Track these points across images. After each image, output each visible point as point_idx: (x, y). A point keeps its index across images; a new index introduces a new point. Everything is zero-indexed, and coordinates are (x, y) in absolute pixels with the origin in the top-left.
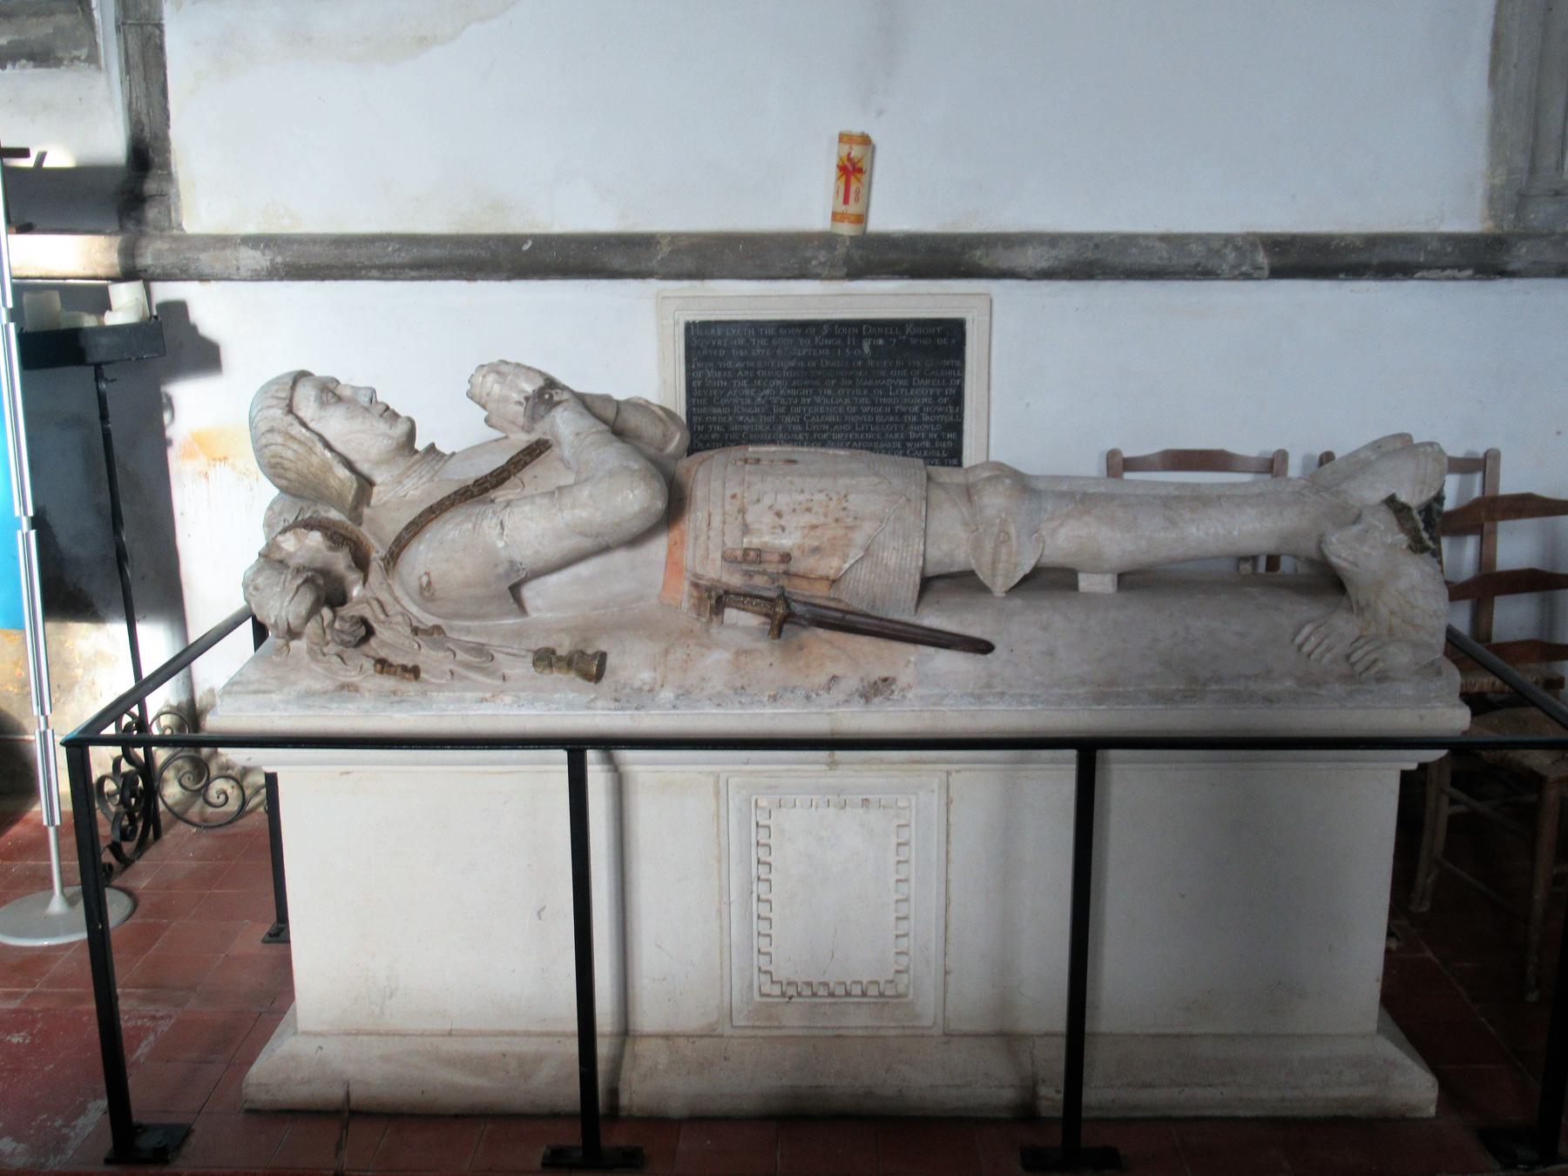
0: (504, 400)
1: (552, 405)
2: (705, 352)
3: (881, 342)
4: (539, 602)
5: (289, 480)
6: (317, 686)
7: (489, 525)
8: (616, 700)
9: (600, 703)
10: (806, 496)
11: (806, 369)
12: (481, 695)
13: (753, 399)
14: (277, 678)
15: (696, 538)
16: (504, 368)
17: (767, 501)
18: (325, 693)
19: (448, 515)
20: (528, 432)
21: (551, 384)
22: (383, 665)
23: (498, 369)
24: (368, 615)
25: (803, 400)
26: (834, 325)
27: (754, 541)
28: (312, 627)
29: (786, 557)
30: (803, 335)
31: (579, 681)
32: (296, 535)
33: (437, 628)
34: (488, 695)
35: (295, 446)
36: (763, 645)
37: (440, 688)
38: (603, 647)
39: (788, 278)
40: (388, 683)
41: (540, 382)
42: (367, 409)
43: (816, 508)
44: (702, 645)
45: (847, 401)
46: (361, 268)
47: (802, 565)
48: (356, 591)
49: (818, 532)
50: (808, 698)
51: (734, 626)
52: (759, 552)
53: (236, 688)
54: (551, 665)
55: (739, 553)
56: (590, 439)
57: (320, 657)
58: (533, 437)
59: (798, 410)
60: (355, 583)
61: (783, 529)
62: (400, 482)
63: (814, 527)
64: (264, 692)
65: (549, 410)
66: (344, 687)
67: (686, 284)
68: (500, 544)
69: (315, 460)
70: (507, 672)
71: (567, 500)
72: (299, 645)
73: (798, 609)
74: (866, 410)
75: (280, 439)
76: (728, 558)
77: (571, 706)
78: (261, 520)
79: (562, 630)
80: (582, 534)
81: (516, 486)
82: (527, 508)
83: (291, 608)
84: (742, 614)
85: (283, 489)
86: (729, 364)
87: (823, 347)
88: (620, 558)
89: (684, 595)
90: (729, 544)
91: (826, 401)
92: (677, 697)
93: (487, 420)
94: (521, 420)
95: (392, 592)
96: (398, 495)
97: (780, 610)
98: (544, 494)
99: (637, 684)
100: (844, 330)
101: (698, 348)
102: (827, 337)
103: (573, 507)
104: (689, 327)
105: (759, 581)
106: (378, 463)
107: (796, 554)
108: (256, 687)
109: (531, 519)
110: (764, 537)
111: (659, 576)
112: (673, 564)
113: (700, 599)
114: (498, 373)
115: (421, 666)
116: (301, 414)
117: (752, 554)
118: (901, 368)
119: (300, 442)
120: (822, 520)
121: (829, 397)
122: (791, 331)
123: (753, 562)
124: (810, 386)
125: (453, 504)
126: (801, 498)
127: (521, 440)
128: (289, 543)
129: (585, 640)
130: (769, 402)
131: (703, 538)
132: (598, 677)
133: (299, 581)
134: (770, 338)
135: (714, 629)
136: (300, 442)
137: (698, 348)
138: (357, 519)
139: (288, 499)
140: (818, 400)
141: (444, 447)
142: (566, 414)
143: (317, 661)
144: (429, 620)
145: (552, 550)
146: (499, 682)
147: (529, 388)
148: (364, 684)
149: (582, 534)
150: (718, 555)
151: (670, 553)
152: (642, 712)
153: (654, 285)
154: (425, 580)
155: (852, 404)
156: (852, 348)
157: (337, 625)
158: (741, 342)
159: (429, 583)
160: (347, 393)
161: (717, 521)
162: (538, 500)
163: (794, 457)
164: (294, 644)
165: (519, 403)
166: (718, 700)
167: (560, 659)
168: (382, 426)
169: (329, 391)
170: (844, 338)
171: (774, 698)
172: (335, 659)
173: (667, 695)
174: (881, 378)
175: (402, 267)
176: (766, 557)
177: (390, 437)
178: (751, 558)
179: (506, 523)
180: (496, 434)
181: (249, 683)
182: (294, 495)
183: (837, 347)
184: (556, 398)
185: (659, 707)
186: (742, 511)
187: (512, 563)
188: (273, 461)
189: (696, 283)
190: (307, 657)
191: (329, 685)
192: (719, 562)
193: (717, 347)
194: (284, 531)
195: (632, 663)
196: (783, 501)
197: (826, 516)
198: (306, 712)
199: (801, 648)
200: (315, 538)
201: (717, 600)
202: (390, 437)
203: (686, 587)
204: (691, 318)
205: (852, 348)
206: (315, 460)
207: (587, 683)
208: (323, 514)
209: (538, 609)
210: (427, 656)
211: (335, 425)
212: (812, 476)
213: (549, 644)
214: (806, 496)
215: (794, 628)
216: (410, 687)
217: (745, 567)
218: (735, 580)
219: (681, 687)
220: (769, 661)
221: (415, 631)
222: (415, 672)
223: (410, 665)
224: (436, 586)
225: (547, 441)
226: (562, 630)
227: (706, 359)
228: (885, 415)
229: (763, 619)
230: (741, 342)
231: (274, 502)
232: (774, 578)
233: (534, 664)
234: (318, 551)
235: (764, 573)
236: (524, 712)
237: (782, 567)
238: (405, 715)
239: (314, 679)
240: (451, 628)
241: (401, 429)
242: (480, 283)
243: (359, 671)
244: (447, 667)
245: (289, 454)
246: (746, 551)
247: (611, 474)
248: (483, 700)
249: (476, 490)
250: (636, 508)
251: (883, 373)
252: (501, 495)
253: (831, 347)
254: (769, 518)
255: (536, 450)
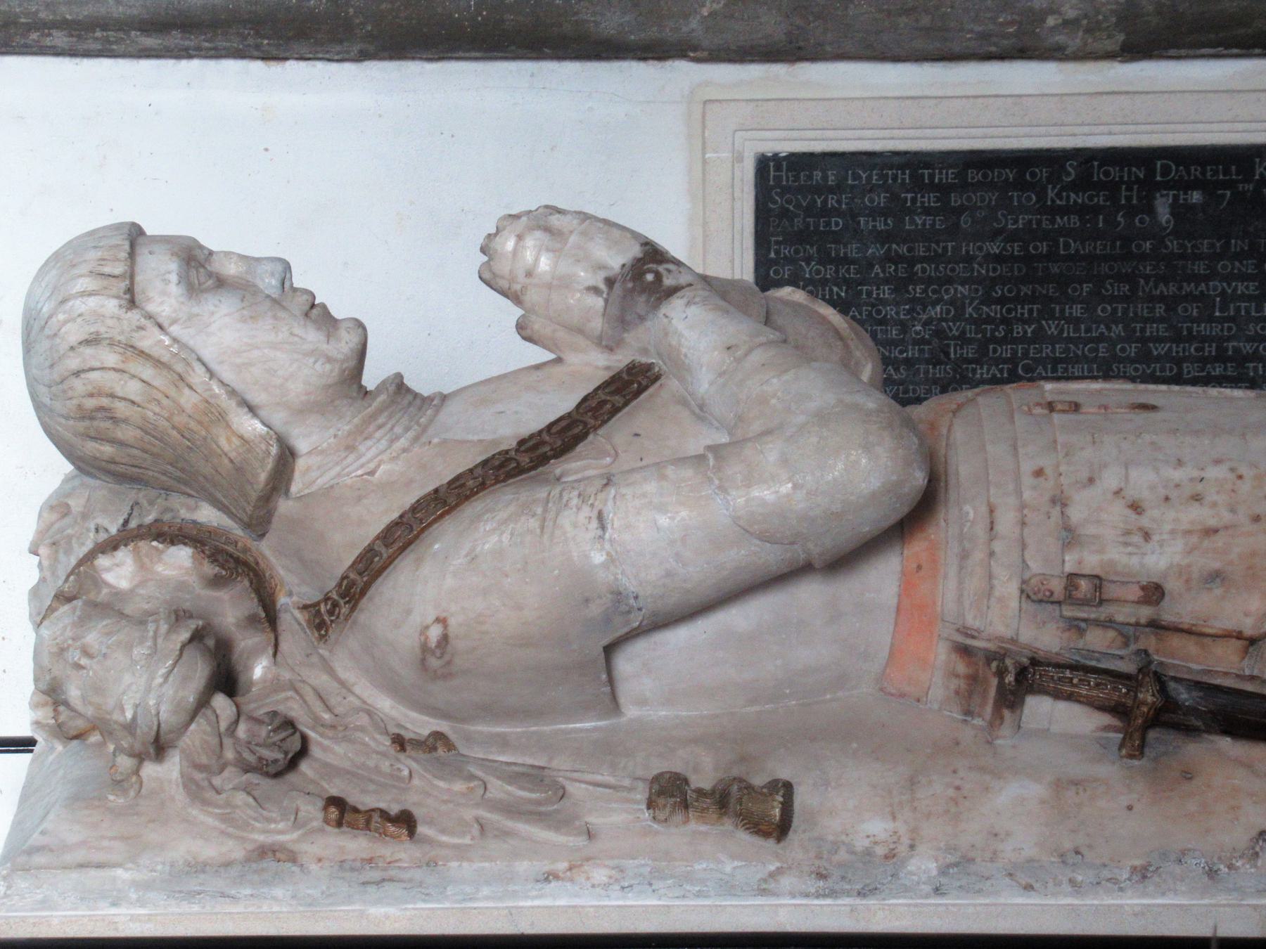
0: (562, 283)
1: (662, 293)
2: (798, 223)
3: (1196, 197)
4: (647, 685)
5: (121, 444)
6: (210, 851)
7: (574, 525)
8: (821, 876)
9: (786, 882)
10: (1188, 472)
11: (1027, 259)
12: (547, 866)
13: (904, 327)
14: (123, 838)
15: (964, 556)
16: (555, 220)
17: (1111, 479)
18: (227, 864)
19: (470, 509)
20: (611, 349)
21: (653, 255)
22: (341, 811)
23: (545, 221)
24: (294, 710)
25: (1018, 330)
26: (1087, 158)
27: (1089, 560)
28: (198, 732)
29: (1154, 593)
30: (1021, 185)
31: (744, 837)
32: (136, 552)
33: (438, 736)
34: (562, 866)
35: (148, 372)
36: (1110, 770)
37: (461, 853)
38: (784, 774)
39: (1002, 57)
40: (356, 844)
41: (636, 251)
42: (275, 302)
43: (1211, 496)
44: (982, 770)
45: (1118, 330)
46: (30, 28)
47: (1183, 607)
48: (259, 670)
49: (1219, 541)
50: (1212, 873)
51: (1044, 733)
52: (1098, 581)
53: (39, 859)
54: (685, 805)
55: (1057, 586)
56: (757, 356)
57: (210, 795)
58: (620, 360)
59: (1006, 351)
60: (256, 653)
61: (1147, 536)
62: (350, 448)
63: (1211, 532)
64: (100, 866)
65: (656, 307)
66: (265, 852)
67: (754, 71)
68: (598, 558)
69: (188, 400)
70: (594, 819)
71: (735, 469)
72: (168, 771)
73: (1184, 696)
74: (1158, 350)
75: (111, 358)
76: (1034, 596)
77: (729, 888)
78: (28, 528)
79: (696, 741)
80: (765, 537)
81: (602, 454)
82: (651, 487)
83: (169, 691)
84: (1062, 706)
85: (84, 465)
86: (853, 250)
87: (1065, 211)
88: (809, 595)
89: (936, 672)
90: (1035, 566)
91: (1068, 331)
92: (943, 872)
93: (521, 327)
94: (597, 324)
95: (331, 672)
96: (351, 481)
97: (1148, 696)
98: (681, 461)
99: (861, 844)
100: (1114, 172)
101: (784, 213)
102: (1074, 187)
103: (749, 483)
104: (767, 167)
105: (1097, 640)
106: (303, 411)
107: (1171, 585)
108: (80, 855)
109: (662, 508)
110: (1108, 551)
111: (882, 634)
112: (913, 609)
113: (973, 679)
114: (547, 229)
115: (418, 813)
116: (151, 308)
117: (1084, 584)
118: (1239, 256)
119: (158, 363)
120: (1227, 517)
121: (1076, 322)
122: (994, 175)
123: (1084, 603)
124: (1032, 299)
125: (483, 486)
126: (1177, 475)
127: (592, 366)
128: (119, 571)
129: (743, 759)
130: (939, 334)
131: (978, 555)
132: (782, 829)
133: (185, 635)
134: (944, 190)
135: (1005, 739)
136: (158, 363)
137: (784, 213)
138: (259, 523)
139: (99, 489)
140: (1051, 329)
141: (421, 383)
142: (694, 311)
143: (205, 802)
144: (421, 725)
145: (698, 572)
146: (581, 841)
147: (617, 259)
148: (304, 847)
149: (765, 537)
150: (1013, 589)
151: (907, 586)
152: (871, 902)
153: (682, 75)
154: (435, 633)
155: (1129, 339)
156: (1131, 212)
157: (242, 730)
158: (881, 199)
159: (445, 639)
160: (231, 269)
161: (1007, 521)
162: (670, 471)
163: (1151, 401)
164: (150, 770)
165: (595, 290)
166: (1027, 877)
167: (700, 793)
168: (312, 336)
169: (194, 261)
170: (1112, 188)
171: (1143, 874)
172: (241, 798)
173: (923, 865)
174: (1196, 278)
175: (124, 25)
176: (1111, 591)
177: (329, 360)
178: (1081, 595)
179: (609, 516)
180: (538, 355)
181: (65, 848)
182: (122, 478)
183: (1096, 210)
184: (668, 281)
185: (906, 890)
186: (1060, 501)
187: (618, 595)
188: (90, 403)
189: (779, 70)
190: (180, 795)
191: (237, 852)
192: (1014, 604)
193: (825, 212)
194: (111, 546)
195: (847, 806)
196: (1143, 481)
197: (1233, 510)
198: (185, 907)
199: (1188, 775)
200: (180, 559)
201: (1012, 679)
202: (329, 360)
203: (942, 654)
204: (769, 148)
205: (1131, 212)
206: (188, 400)
207: (758, 841)
208: (184, 513)
209: (642, 702)
210: (424, 789)
211: (220, 334)
212: (1197, 433)
213: (675, 765)
214: (1188, 472)
215: (1170, 736)
216: (400, 851)
217: (1068, 612)
218: (1046, 637)
219: (951, 849)
220: (1124, 800)
221: (400, 743)
222: (406, 821)
223: (394, 809)
224: (458, 644)
225: (649, 367)
226: (696, 741)
227: (802, 237)
228: (1204, 361)
229: (1106, 719)
230: (881, 199)
231: (58, 507)
232: (1126, 633)
233: (650, 805)
234: (181, 586)
235: (1108, 624)
236: (631, 900)
237: (1145, 613)
238: (391, 910)
239: (199, 838)
240: (468, 738)
241: (346, 343)
242: (291, 65)
243: (291, 819)
244: (469, 814)
245: (132, 389)
246: (1072, 578)
247: (822, 418)
248: (549, 877)
249: (525, 460)
250: (875, 483)
251: (1200, 268)
252: (575, 466)
253: (1081, 210)
254: (1117, 513)
255: (627, 387)
